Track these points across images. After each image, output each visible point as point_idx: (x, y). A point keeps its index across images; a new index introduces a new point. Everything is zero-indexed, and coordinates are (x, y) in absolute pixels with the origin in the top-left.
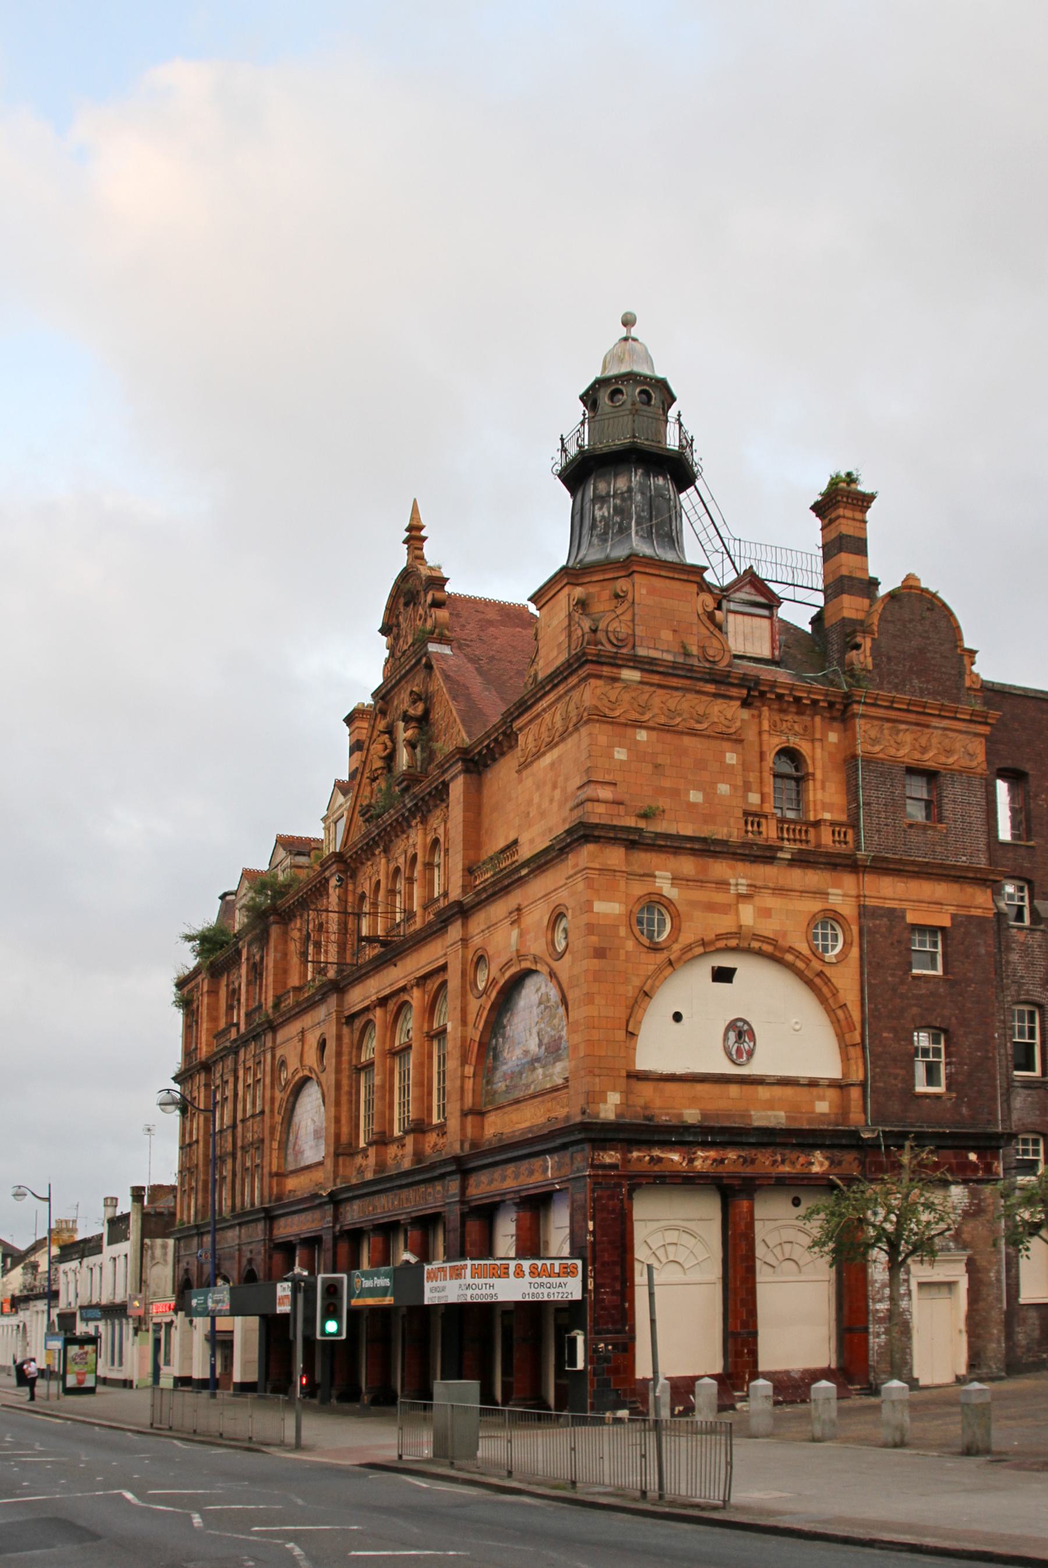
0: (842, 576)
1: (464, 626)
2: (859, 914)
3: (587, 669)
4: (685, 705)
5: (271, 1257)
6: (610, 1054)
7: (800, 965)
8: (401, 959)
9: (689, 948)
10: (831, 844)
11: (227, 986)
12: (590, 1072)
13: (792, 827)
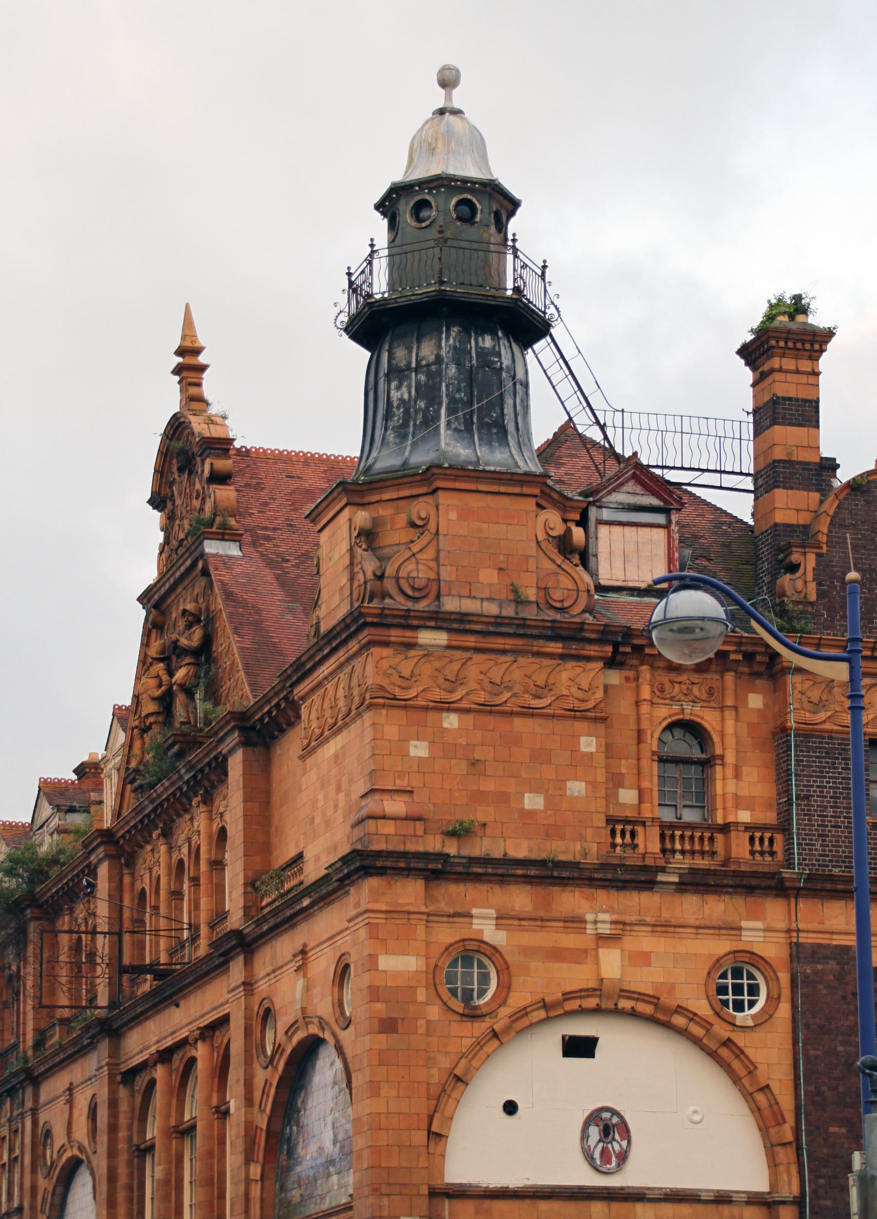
0: (775, 461)
1: (266, 504)
2: (791, 955)
3: (365, 636)
4: (516, 675)
6: (404, 1164)
7: (696, 1030)
8: (184, 997)
9: (524, 1012)
10: (747, 856)
12: (375, 1190)
13: (688, 833)
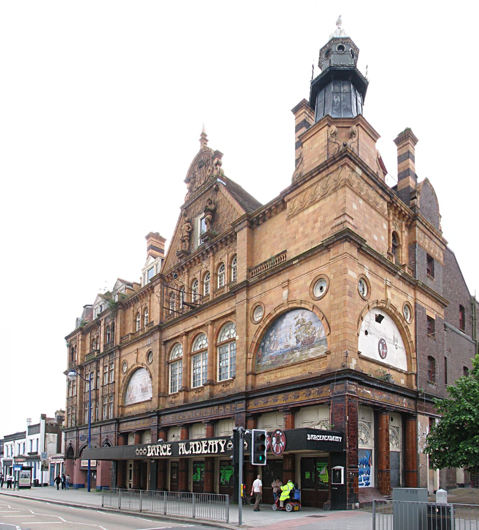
5: (118, 438)
11: (90, 337)
